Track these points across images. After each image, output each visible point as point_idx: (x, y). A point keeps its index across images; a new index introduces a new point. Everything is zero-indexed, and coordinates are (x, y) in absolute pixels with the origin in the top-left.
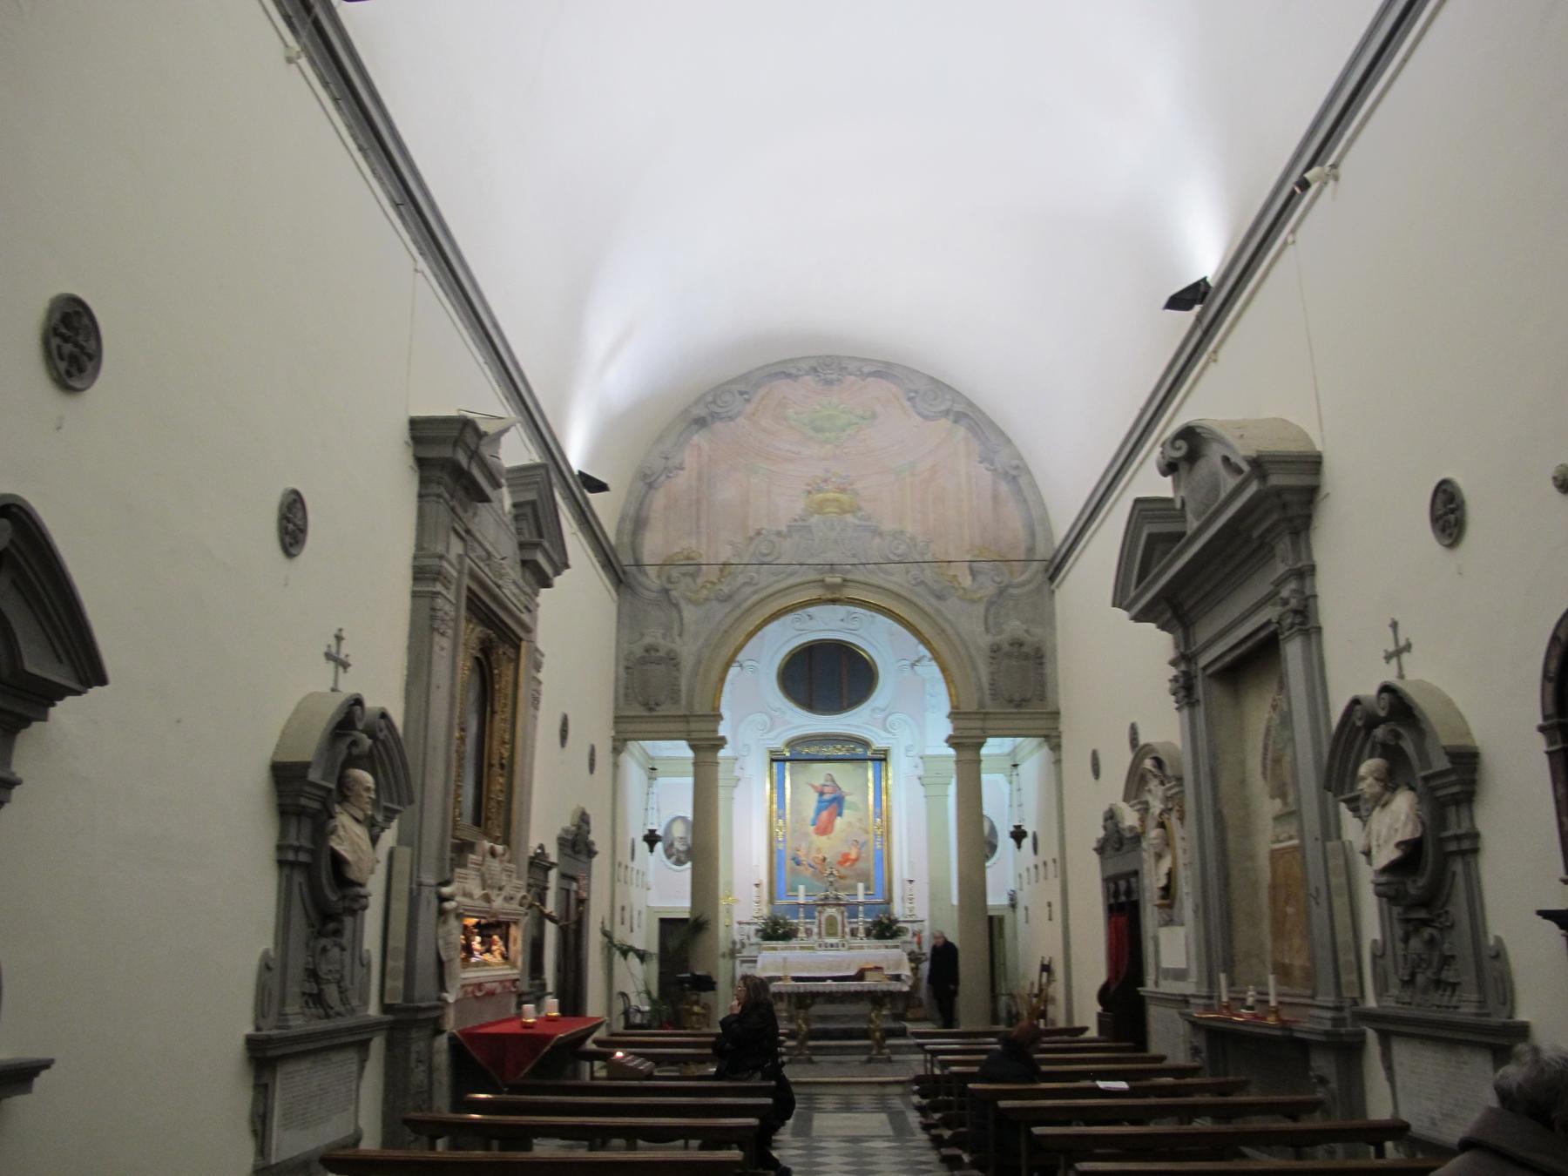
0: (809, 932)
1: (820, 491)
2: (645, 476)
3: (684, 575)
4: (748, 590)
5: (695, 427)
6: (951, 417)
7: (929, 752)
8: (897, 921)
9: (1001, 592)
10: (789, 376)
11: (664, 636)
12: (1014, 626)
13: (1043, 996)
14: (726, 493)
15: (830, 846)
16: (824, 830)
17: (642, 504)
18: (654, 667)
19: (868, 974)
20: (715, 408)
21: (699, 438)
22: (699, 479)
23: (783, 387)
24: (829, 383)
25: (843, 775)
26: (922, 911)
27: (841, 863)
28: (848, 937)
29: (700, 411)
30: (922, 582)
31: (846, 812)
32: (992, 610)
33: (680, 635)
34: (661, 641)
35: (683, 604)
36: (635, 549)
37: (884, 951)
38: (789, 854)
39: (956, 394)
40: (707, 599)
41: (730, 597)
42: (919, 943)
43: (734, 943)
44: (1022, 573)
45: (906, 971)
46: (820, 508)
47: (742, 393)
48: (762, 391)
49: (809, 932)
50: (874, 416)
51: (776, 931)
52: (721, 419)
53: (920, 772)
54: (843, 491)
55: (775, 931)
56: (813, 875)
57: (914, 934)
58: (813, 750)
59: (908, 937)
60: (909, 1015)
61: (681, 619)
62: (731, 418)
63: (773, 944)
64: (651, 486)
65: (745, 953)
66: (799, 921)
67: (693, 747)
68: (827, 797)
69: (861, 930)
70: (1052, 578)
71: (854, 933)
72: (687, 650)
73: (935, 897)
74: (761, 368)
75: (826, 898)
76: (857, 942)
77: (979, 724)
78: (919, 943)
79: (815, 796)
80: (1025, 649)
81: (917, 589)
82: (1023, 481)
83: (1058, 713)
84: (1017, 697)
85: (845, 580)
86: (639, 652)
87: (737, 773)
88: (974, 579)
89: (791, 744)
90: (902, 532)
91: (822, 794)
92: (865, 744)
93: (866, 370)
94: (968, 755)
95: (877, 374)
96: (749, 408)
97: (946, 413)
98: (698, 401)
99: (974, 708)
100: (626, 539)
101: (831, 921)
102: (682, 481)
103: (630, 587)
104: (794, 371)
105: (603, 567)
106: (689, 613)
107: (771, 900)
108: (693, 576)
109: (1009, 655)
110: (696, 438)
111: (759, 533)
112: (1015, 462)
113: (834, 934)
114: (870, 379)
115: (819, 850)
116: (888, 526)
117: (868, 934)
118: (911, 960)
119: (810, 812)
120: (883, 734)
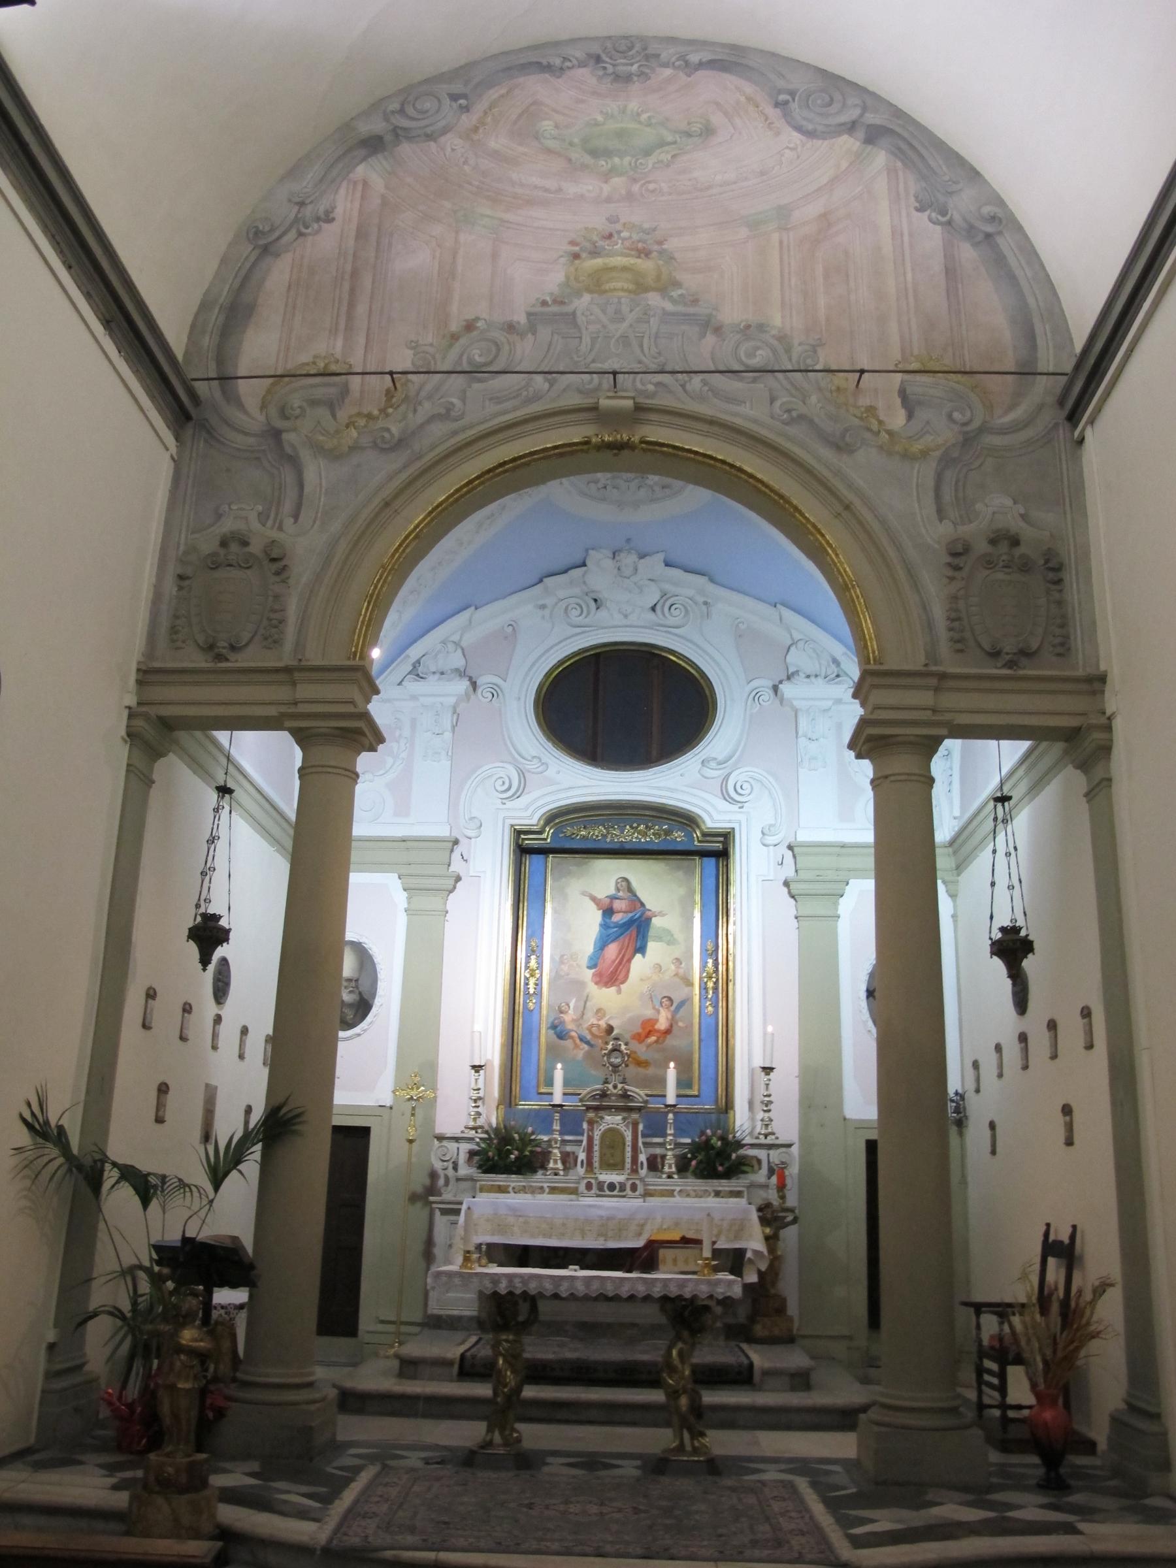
0: (568, 1160)
1: (595, 253)
2: (258, 233)
3: (314, 403)
4: (438, 430)
5: (362, 152)
6: (861, 134)
7: (803, 836)
8: (739, 1145)
9: (968, 440)
10: (548, 68)
11: (263, 518)
12: (997, 507)
13: (1066, 1314)
14: (414, 259)
15: (620, 1005)
16: (613, 976)
17: (246, 278)
18: (235, 573)
19: (662, 1253)
20: (405, 123)
21: (371, 171)
22: (361, 234)
23: (535, 86)
24: (628, 79)
25: (658, 888)
26: (787, 1127)
27: (640, 1038)
28: (643, 1172)
29: (376, 126)
30: (802, 417)
31: (651, 946)
32: (950, 475)
33: (296, 517)
34: (255, 525)
35: (305, 455)
36: (224, 351)
37: (711, 1202)
38: (545, 1015)
39: (868, 97)
40: (355, 448)
41: (400, 443)
42: (781, 1187)
43: (433, 1175)
44: (1012, 407)
45: (754, 1243)
46: (596, 283)
47: (454, 97)
48: (494, 94)
49: (568, 1160)
50: (708, 131)
51: (507, 1154)
52: (410, 139)
53: (789, 871)
54: (645, 253)
55: (503, 1154)
56: (588, 1055)
57: (771, 1172)
58: (597, 833)
59: (761, 1176)
60: (759, 1330)
61: (301, 485)
62: (430, 137)
63: (500, 1179)
64: (266, 250)
65: (447, 1196)
66: (552, 1137)
67: (302, 738)
68: (617, 918)
69: (670, 1159)
70: (1073, 418)
71: (654, 1164)
72: (306, 544)
73: (818, 1088)
74: (494, 57)
75: (604, 1095)
76: (659, 1182)
77: (925, 698)
78: (781, 1187)
79: (597, 916)
80: (1022, 550)
81: (792, 430)
82: (1006, 243)
83: (1102, 679)
84: (1009, 646)
85: (639, 408)
86: (208, 545)
87: (457, 866)
88: (910, 416)
89: (553, 818)
90: (761, 327)
91: (608, 912)
92: (687, 820)
93: (694, 58)
94: (902, 763)
95: (712, 64)
96: (466, 121)
97: (851, 128)
98: (375, 106)
99: (916, 663)
100: (207, 341)
101: (613, 1140)
102: (326, 242)
103: (205, 427)
104: (557, 62)
105: (107, 323)
106: (315, 472)
107: (508, 1098)
108: (332, 406)
109: (989, 562)
110: (361, 170)
111: (469, 326)
112: (987, 210)
113: (617, 1166)
114: (700, 73)
115: (600, 1012)
116: (732, 314)
117: (683, 1167)
118: (764, 1221)
119: (587, 946)
120: (723, 805)
